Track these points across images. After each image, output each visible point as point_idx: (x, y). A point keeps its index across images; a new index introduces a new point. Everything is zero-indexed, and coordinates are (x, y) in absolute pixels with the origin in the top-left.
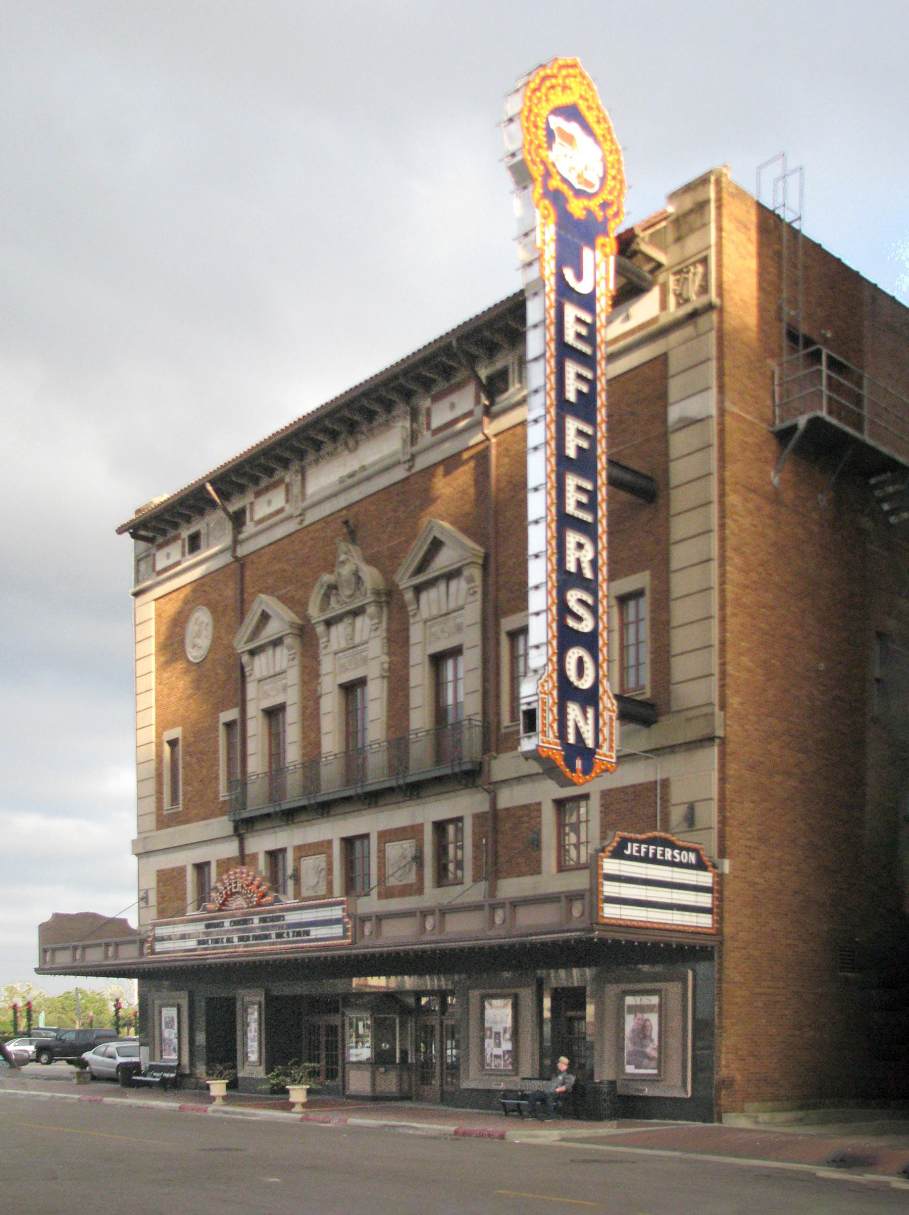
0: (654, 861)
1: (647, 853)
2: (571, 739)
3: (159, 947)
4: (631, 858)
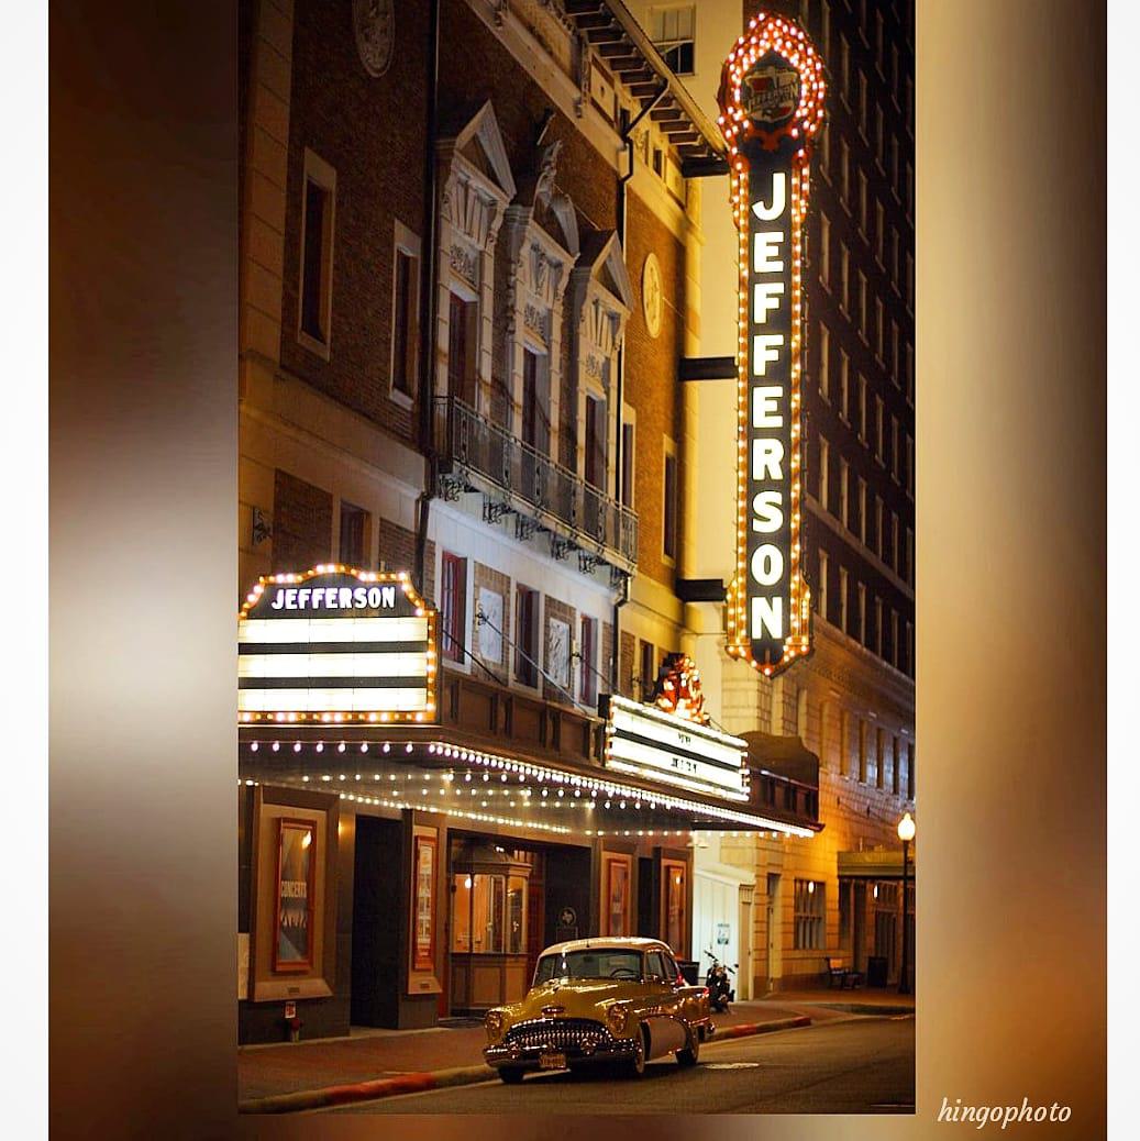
0: (323, 612)
1: (309, 603)
4: (284, 614)
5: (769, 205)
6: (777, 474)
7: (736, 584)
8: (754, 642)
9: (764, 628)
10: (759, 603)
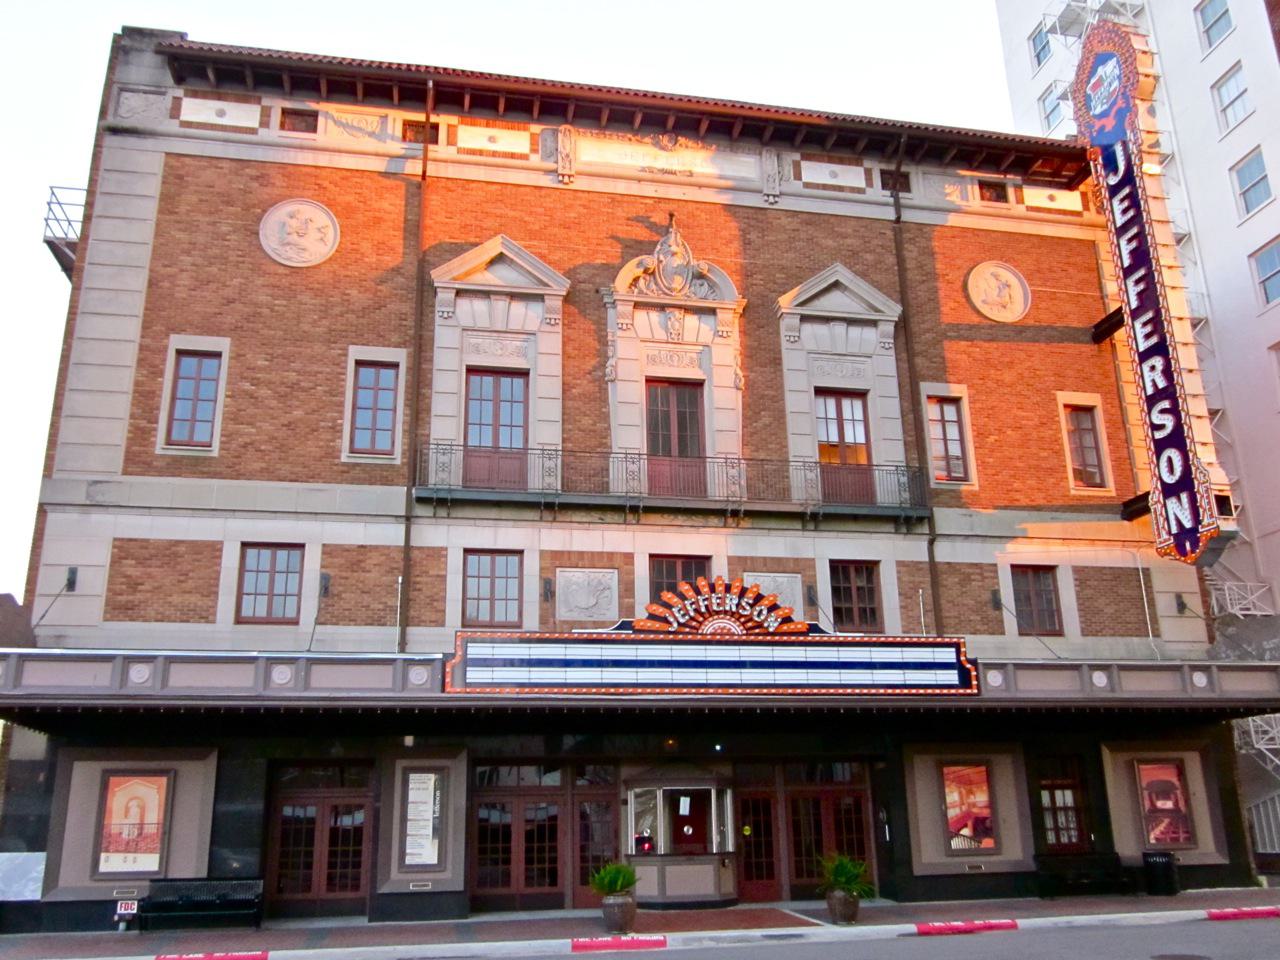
2: (1174, 530)
3: (475, 675)
5: (1115, 170)
6: (1161, 384)
7: (1156, 498)
8: (1175, 536)
9: (1179, 499)
10: (1172, 503)
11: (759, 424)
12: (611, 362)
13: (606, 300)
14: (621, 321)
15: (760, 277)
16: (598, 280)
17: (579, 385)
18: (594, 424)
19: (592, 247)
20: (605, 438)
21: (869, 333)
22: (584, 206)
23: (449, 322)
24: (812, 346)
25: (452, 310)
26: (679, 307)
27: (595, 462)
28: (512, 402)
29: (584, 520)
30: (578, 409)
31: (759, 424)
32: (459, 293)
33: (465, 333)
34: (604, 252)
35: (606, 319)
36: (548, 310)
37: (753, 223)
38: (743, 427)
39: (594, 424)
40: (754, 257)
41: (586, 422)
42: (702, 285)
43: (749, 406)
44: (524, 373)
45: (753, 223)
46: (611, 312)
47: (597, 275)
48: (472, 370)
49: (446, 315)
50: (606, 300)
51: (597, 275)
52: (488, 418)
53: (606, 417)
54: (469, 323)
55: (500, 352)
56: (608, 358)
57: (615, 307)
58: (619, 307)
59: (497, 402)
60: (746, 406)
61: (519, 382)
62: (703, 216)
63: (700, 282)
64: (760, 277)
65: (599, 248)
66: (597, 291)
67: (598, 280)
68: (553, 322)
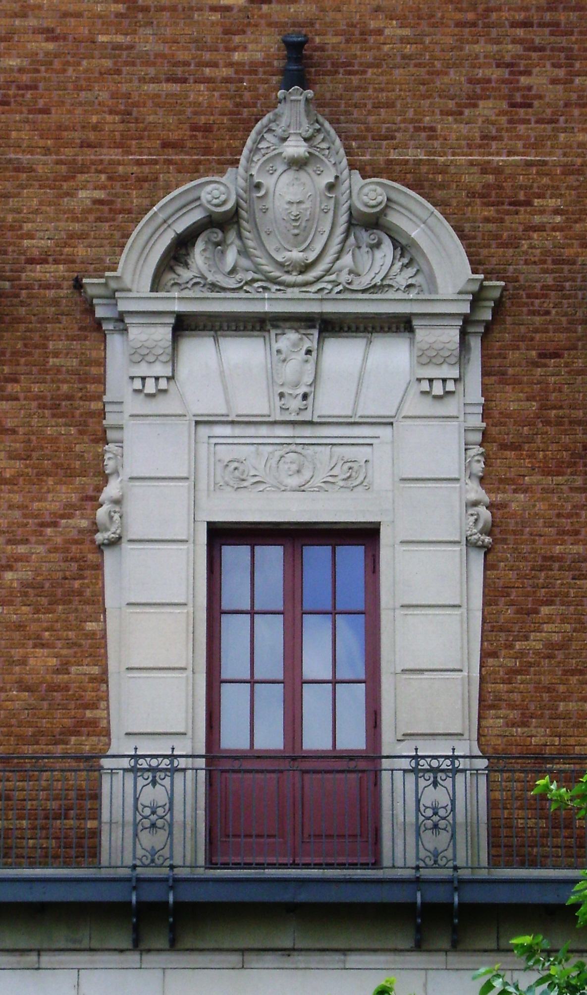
11: (535, 643)
12: (112, 490)
13: (100, 313)
14: (143, 370)
15: (552, 203)
16: (81, 251)
17: (23, 558)
18: (63, 669)
19: (68, 153)
20: (94, 706)
21: (392, 357)
22: (50, 34)
23: (161, 406)
24: (210, 403)
25: (162, 370)
26: (304, 322)
27: (80, 779)
28: (252, 613)
29: (22, 945)
30: (20, 627)
31: (535, 643)
32: (184, 325)
33: (204, 431)
34: (101, 167)
35: (101, 363)
36: (425, 358)
37: (540, 36)
38: (486, 655)
39: (63, 669)
40: (536, 145)
41: (42, 662)
42: (378, 245)
43: (505, 591)
44: (367, 535)
45: (540, 36)
46: (116, 347)
47: (83, 236)
48: (220, 535)
49: (150, 387)
50: (100, 313)
51: (83, 236)
52: (271, 664)
53: (96, 648)
54: (215, 406)
55: (294, 481)
56: (106, 479)
57: (125, 330)
58: (133, 332)
59: (294, 614)
60: (492, 595)
61: (352, 556)
62: (393, 30)
63: (366, 237)
64: (552, 203)
65: (90, 155)
66: (78, 285)
67: (81, 251)
68: (438, 389)
